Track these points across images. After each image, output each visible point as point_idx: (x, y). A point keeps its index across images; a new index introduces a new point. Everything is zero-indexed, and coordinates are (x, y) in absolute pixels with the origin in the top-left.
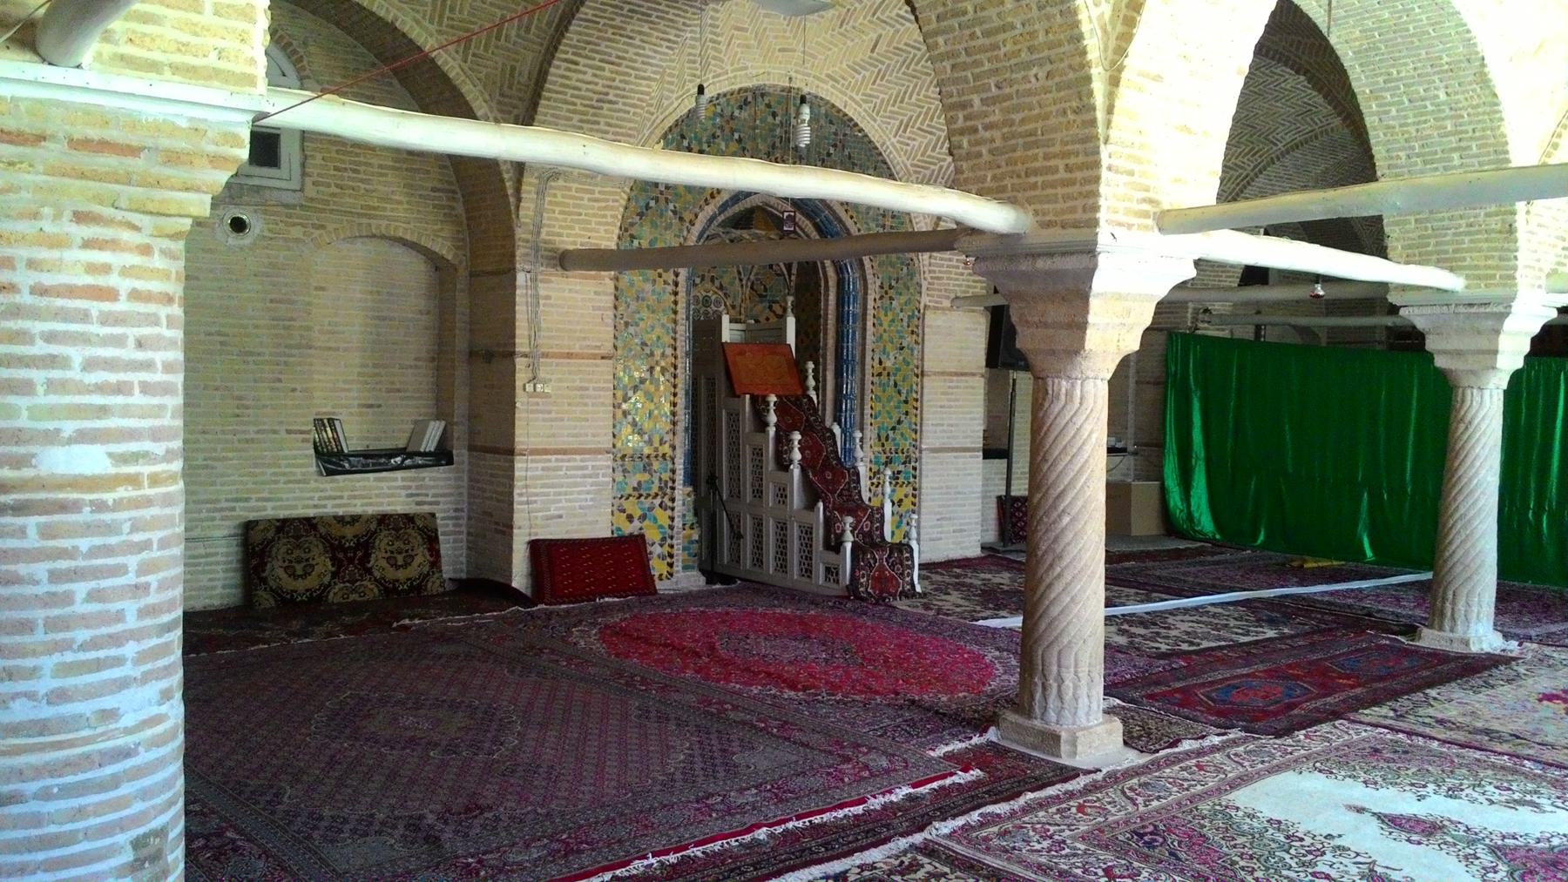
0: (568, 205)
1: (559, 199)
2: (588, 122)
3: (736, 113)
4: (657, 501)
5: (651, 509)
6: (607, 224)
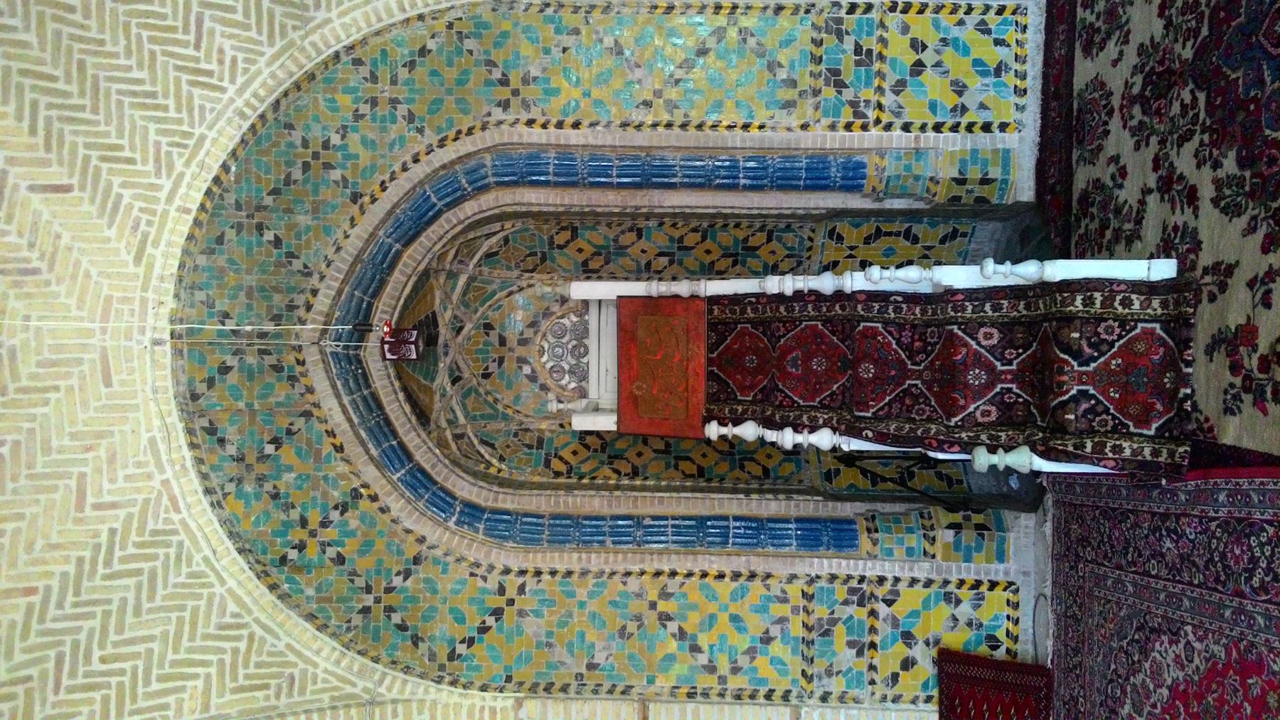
3: (231, 450)
4: (882, 609)
5: (895, 623)
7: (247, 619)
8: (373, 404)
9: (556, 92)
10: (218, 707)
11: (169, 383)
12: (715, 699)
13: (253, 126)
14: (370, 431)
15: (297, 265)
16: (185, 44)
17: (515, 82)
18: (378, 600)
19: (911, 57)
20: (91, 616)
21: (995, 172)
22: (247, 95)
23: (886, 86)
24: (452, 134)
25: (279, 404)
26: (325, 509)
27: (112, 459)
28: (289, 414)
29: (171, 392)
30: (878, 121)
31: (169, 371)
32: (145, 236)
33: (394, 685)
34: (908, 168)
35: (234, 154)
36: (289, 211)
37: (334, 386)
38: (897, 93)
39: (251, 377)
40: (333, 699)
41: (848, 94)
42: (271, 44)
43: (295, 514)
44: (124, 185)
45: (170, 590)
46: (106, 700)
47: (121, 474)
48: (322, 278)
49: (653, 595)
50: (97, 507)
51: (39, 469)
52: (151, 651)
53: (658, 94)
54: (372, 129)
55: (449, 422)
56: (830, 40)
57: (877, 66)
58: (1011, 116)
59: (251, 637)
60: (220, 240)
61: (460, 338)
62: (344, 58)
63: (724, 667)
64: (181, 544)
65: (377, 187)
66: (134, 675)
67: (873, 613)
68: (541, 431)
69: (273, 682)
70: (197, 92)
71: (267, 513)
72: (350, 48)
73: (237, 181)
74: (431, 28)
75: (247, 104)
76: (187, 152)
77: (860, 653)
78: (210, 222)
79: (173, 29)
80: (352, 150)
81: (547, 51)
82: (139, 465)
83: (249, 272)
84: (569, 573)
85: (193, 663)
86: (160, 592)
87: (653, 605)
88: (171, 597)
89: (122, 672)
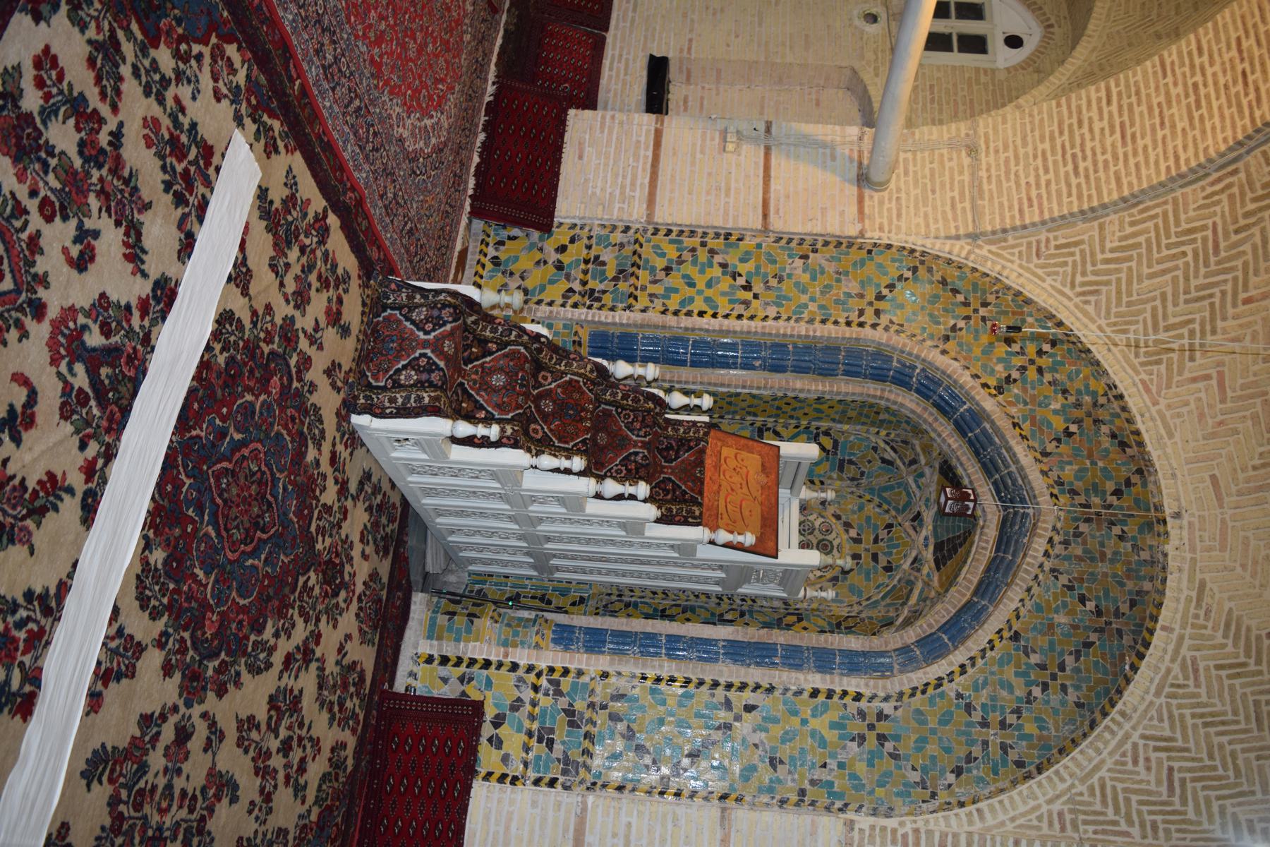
0: (942, 175)
1: (947, 165)
2: (1045, 159)
3: (1105, 429)
4: (577, 286)
5: (568, 277)
6: (927, 226)
7: (1077, 300)
8: (989, 468)
9: (833, 725)
10: (1092, 228)
11: (1163, 483)
12: (711, 231)
13: (1113, 706)
14: (992, 442)
15: (1064, 579)
16: (1181, 770)
17: (872, 738)
18: (976, 311)
19: (504, 731)
20: (1198, 288)
21: (442, 619)
22: (1121, 734)
23: (528, 707)
24: (930, 691)
25: (1070, 463)
26: (1024, 381)
27: (1201, 416)
28: (1061, 455)
29: (1160, 474)
30: (539, 675)
31: (1164, 492)
32: (1198, 605)
33: (959, 250)
34: (516, 634)
35: (1128, 681)
36: (1075, 627)
37: (1024, 478)
38: (519, 700)
39: (1095, 486)
40: (1005, 240)
41: (563, 702)
42: (1102, 779)
43: (1048, 377)
44: (1224, 646)
45: (1141, 318)
46: (1177, 224)
47: (1193, 406)
48: (1041, 566)
49: (755, 303)
50: (1207, 377)
51: (1258, 401)
52: (1149, 267)
53: (738, 718)
54: (1003, 699)
55: (922, 475)
56: (575, 755)
57: (535, 726)
58: (422, 669)
59: (1073, 285)
60: (1133, 604)
61: (914, 554)
62: (1032, 768)
63: (702, 255)
64: (1137, 355)
65: (997, 643)
66: (1159, 246)
67: (584, 283)
68: (841, 479)
69: (1052, 251)
70: (1167, 733)
71: (1070, 378)
72: (1028, 777)
73: (1122, 657)
74: (952, 794)
75: (1119, 724)
76: (1170, 680)
77: (597, 258)
78: (1143, 619)
79: (1194, 780)
80: (1022, 680)
81: (841, 766)
82: (1179, 415)
83: (1105, 575)
84: (823, 322)
85: (1116, 261)
86: (1148, 315)
87: (756, 296)
88: (1139, 313)
89: (1168, 247)
